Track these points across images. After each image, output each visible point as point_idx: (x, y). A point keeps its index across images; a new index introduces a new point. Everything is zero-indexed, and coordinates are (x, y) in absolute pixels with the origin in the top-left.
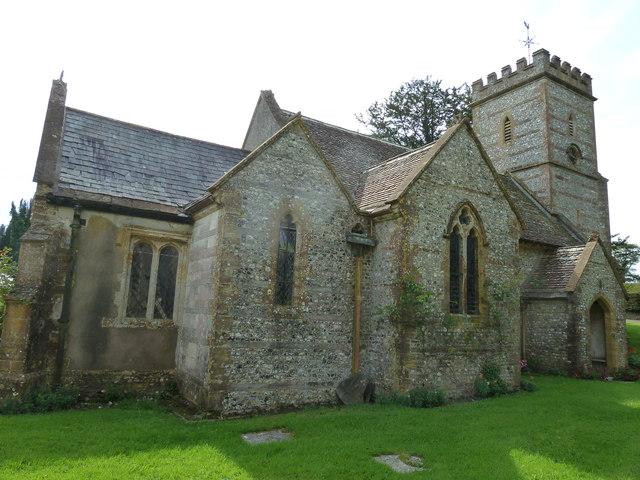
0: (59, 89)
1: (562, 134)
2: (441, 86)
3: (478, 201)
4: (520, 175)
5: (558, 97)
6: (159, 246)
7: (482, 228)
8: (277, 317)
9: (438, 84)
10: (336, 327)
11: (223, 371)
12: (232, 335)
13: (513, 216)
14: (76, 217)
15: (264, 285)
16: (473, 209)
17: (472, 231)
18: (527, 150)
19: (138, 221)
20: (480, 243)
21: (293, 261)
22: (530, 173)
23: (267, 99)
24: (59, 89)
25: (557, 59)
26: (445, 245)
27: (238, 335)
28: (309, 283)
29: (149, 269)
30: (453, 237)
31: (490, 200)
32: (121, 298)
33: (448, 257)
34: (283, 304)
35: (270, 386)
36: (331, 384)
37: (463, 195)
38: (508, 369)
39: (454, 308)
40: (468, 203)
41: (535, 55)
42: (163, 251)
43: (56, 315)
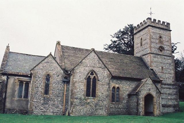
0: (8, 47)
1: (156, 43)
2: (121, 30)
3: (96, 70)
4: (144, 57)
5: (155, 32)
6: (25, 83)
7: (97, 76)
8: (44, 97)
9: (120, 30)
10: (59, 100)
11: (32, 108)
12: (34, 100)
13: (109, 73)
14: (8, 77)
15: (42, 90)
16: (95, 72)
17: (95, 77)
18: (146, 49)
19: (20, 78)
20: (97, 80)
21: (49, 85)
22: (146, 56)
23: (58, 43)
24: (8, 47)
25: (155, 20)
26: (85, 81)
27: (35, 101)
28: (52, 90)
29: (90, 90)
30: (88, 79)
31: (101, 69)
32: (16, 93)
33: (86, 84)
34: (46, 95)
35: (42, 112)
36: (57, 113)
37: (91, 68)
38: (105, 111)
39: (88, 95)
40: (93, 70)
41: (147, 19)
42: (25, 83)
43: (4, 97)
